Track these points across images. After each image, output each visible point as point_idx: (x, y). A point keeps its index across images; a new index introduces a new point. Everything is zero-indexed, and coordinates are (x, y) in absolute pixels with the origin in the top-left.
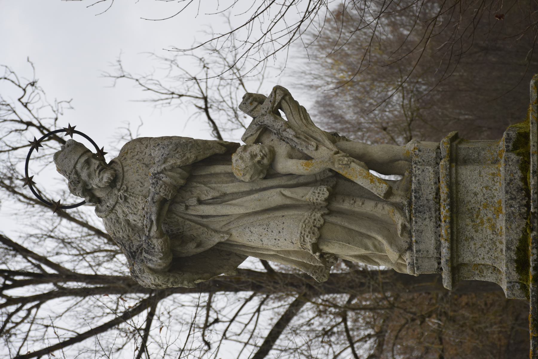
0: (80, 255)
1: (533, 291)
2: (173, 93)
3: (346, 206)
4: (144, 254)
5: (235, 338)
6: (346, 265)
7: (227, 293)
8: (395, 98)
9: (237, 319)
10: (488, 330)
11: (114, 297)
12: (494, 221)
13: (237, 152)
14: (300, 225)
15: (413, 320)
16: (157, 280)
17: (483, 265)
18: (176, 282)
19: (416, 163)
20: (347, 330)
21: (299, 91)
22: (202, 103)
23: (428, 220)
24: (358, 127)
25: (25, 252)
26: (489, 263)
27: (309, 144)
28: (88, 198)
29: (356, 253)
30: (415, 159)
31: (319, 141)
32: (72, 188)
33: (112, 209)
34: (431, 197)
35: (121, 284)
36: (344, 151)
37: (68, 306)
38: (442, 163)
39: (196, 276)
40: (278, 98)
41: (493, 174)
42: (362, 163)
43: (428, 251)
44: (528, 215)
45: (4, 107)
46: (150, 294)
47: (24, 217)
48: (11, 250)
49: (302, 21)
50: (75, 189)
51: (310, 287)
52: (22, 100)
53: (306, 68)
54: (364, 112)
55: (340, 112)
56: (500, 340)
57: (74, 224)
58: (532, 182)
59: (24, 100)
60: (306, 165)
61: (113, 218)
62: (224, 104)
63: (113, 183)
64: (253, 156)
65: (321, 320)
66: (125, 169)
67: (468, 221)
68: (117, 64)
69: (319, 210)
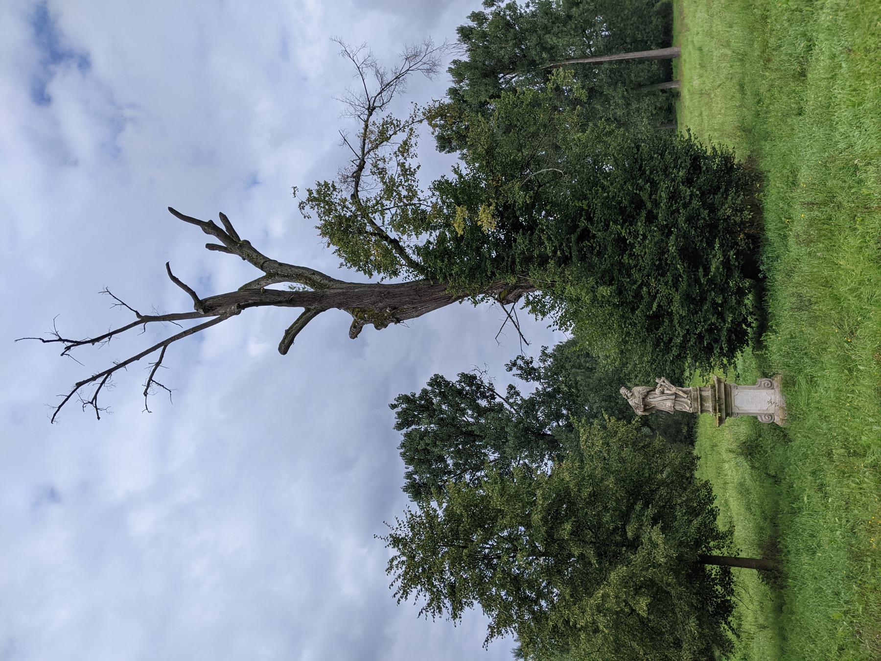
3: (678, 399)
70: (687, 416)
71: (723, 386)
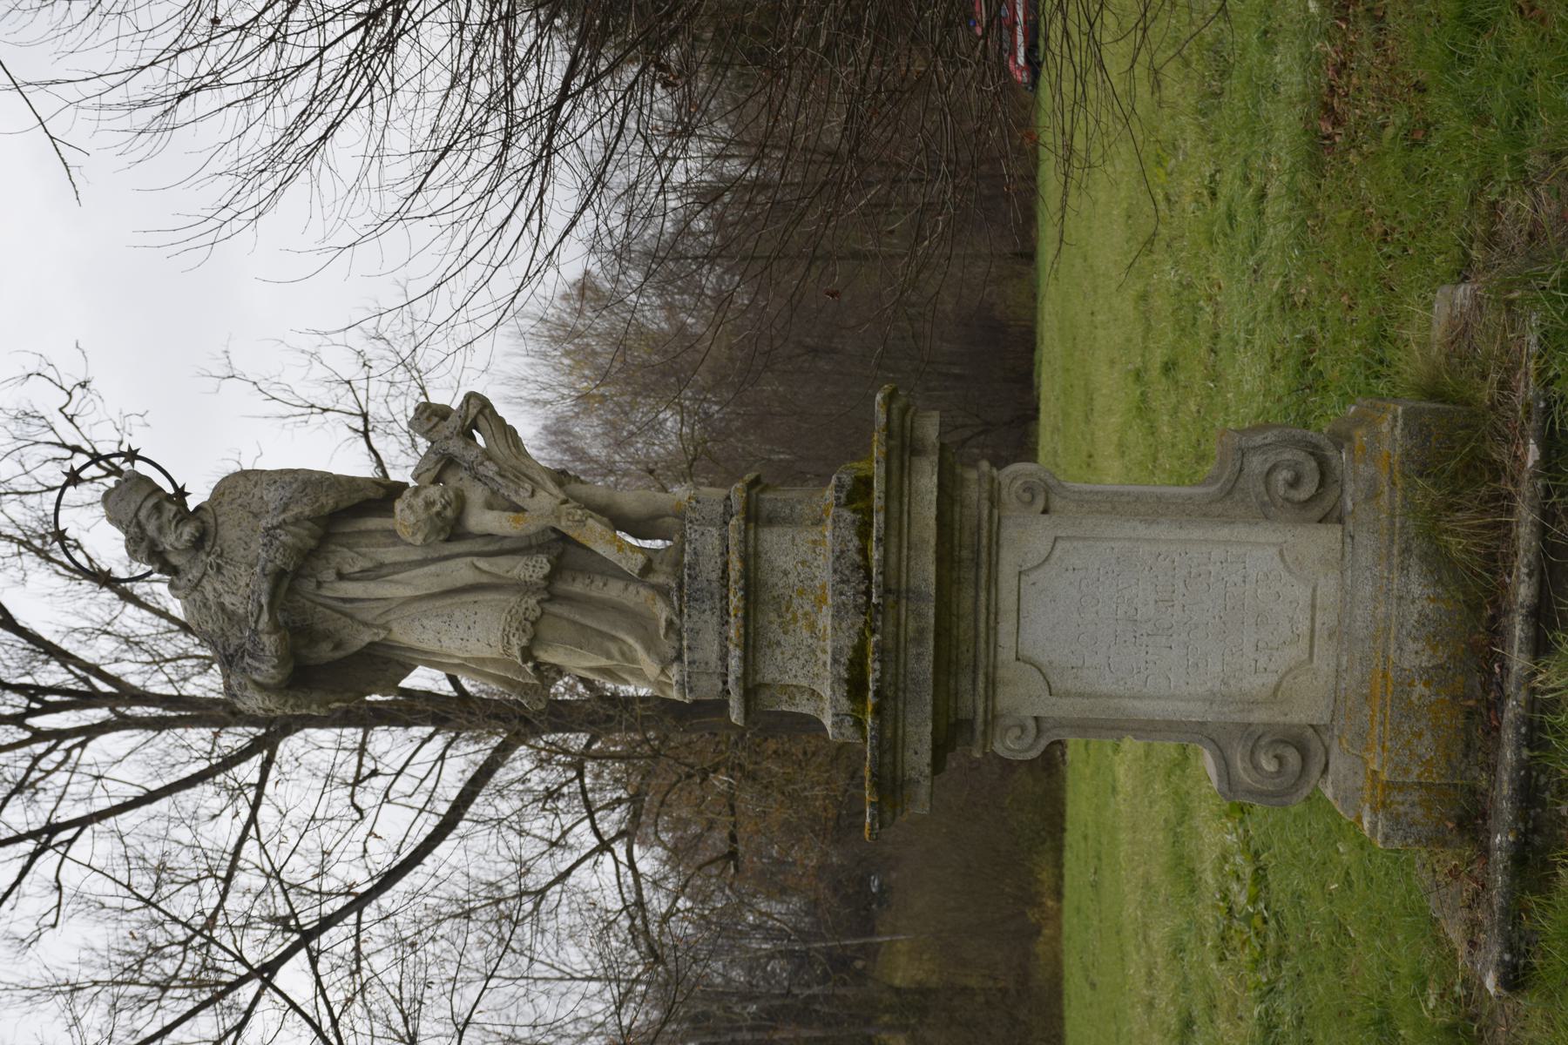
0: (155, 662)
1: (872, 729)
2: (312, 406)
3: (578, 587)
4: (247, 659)
5: (402, 800)
6: (585, 687)
7: (393, 728)
8: (669, 424)
9: (407, 770)
10: (806, 793)
11: (207, 732)
12: (813, 617)
13: (404, 497)
14: (503, 617)
15: (689, 776)
16: (267, 702)
17: (795, 686)
18: (298, 706)
19: (691, 522)
20: (584, 792)
21: (517, 408)
22: (358, 423)
23: (708, 613)
24: (609, 469)
25: (64, 657)
26: (804, 683)
27: (520, 486)
28: (157, 566)
29: (593, 664)
30: (689, 514)
31: (537, 483)
32: (132, 549)
33: (197, 585)
34: (714, 576)
35: (220, 711)
36: (576, 499)
37: (133, 746)
38: (733, 522)
39: (332, 697)
40: (473, 411)
41: (814, 542)
42: (605, 519)
43: (707, 663)
44: (868, 607)
45: (36, 421)
46: (268, 729)
47: (64, 599)
48: (40, 653)
49: (519, 291)
50: (135, 551)
51: (526, 721)
52: (65, 410)
53: (529, 373)
54: (619, 444)
55: (581, 444)
56: (825, 810)
57: (145, 613)
58: (876, 555)
59: (68, 411)
60: (514, 520)
61: (198, 599)
62: (395, 425)
63: (198, 543)
64: (429, 504)
65: (543, 774)
66: (220, 520)
67: (773, 616)
68: (224, 356)
69: (534, 593)
70: (330, 486)
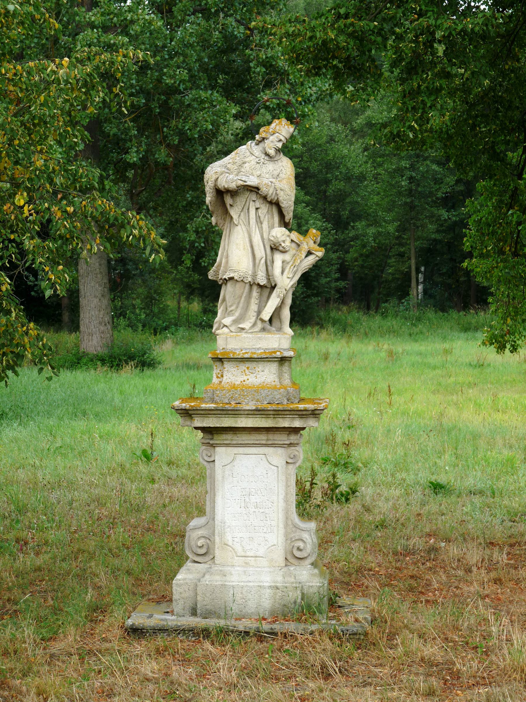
71: (297, 424)
